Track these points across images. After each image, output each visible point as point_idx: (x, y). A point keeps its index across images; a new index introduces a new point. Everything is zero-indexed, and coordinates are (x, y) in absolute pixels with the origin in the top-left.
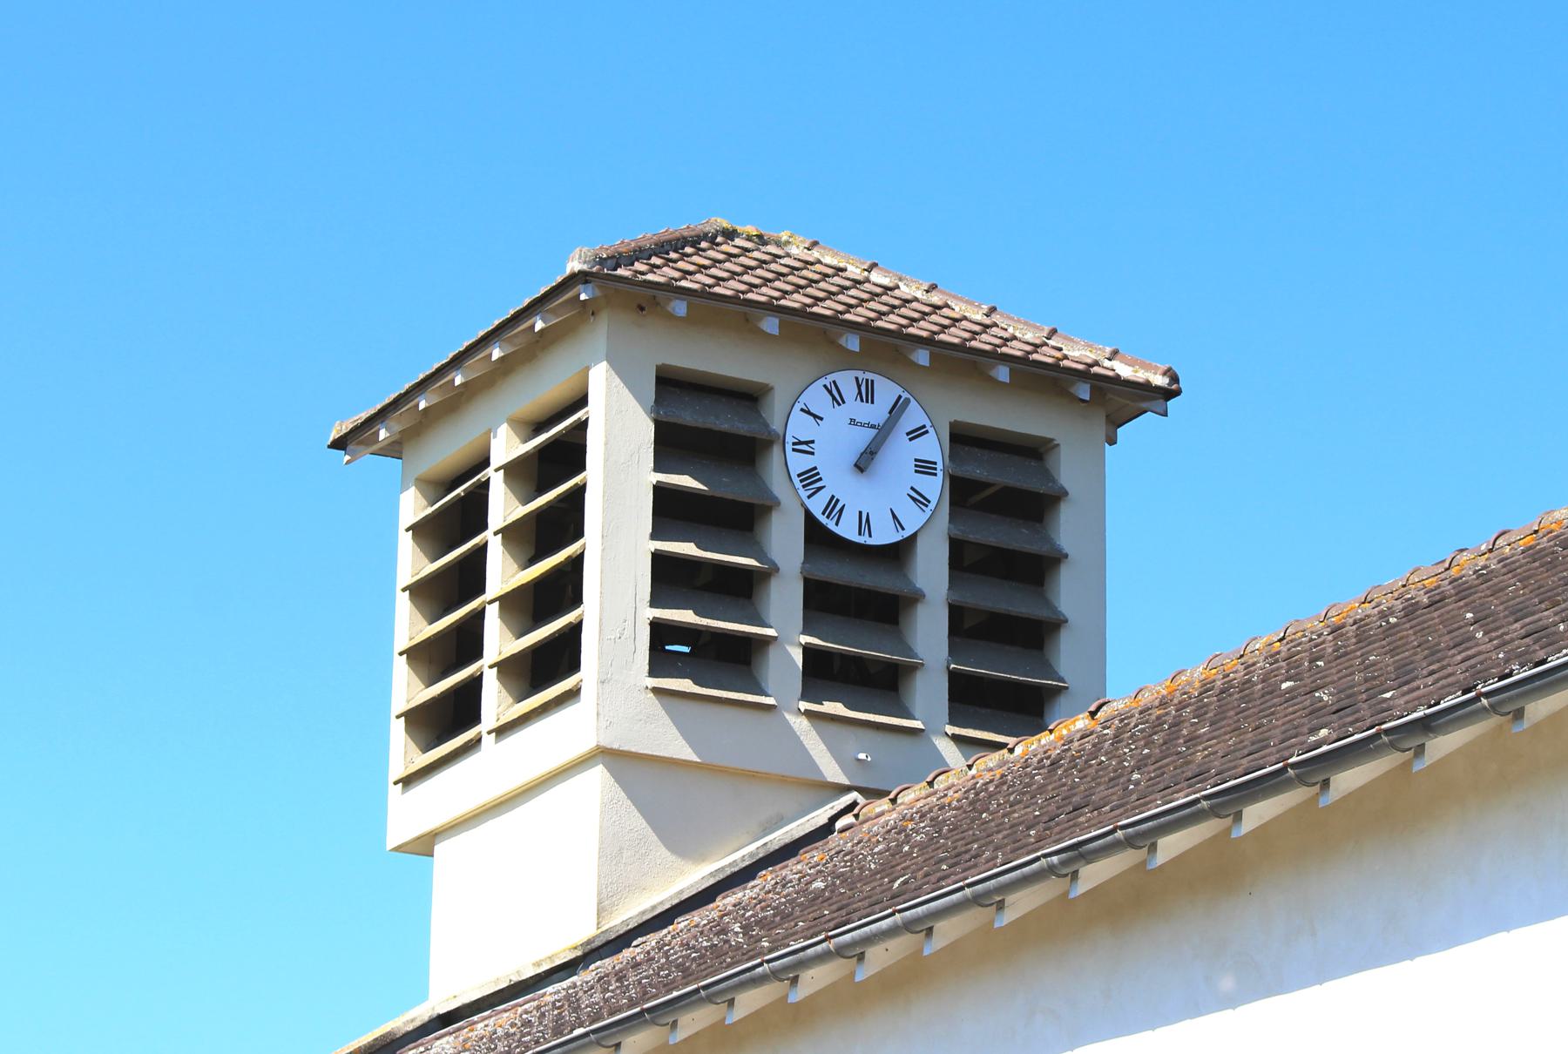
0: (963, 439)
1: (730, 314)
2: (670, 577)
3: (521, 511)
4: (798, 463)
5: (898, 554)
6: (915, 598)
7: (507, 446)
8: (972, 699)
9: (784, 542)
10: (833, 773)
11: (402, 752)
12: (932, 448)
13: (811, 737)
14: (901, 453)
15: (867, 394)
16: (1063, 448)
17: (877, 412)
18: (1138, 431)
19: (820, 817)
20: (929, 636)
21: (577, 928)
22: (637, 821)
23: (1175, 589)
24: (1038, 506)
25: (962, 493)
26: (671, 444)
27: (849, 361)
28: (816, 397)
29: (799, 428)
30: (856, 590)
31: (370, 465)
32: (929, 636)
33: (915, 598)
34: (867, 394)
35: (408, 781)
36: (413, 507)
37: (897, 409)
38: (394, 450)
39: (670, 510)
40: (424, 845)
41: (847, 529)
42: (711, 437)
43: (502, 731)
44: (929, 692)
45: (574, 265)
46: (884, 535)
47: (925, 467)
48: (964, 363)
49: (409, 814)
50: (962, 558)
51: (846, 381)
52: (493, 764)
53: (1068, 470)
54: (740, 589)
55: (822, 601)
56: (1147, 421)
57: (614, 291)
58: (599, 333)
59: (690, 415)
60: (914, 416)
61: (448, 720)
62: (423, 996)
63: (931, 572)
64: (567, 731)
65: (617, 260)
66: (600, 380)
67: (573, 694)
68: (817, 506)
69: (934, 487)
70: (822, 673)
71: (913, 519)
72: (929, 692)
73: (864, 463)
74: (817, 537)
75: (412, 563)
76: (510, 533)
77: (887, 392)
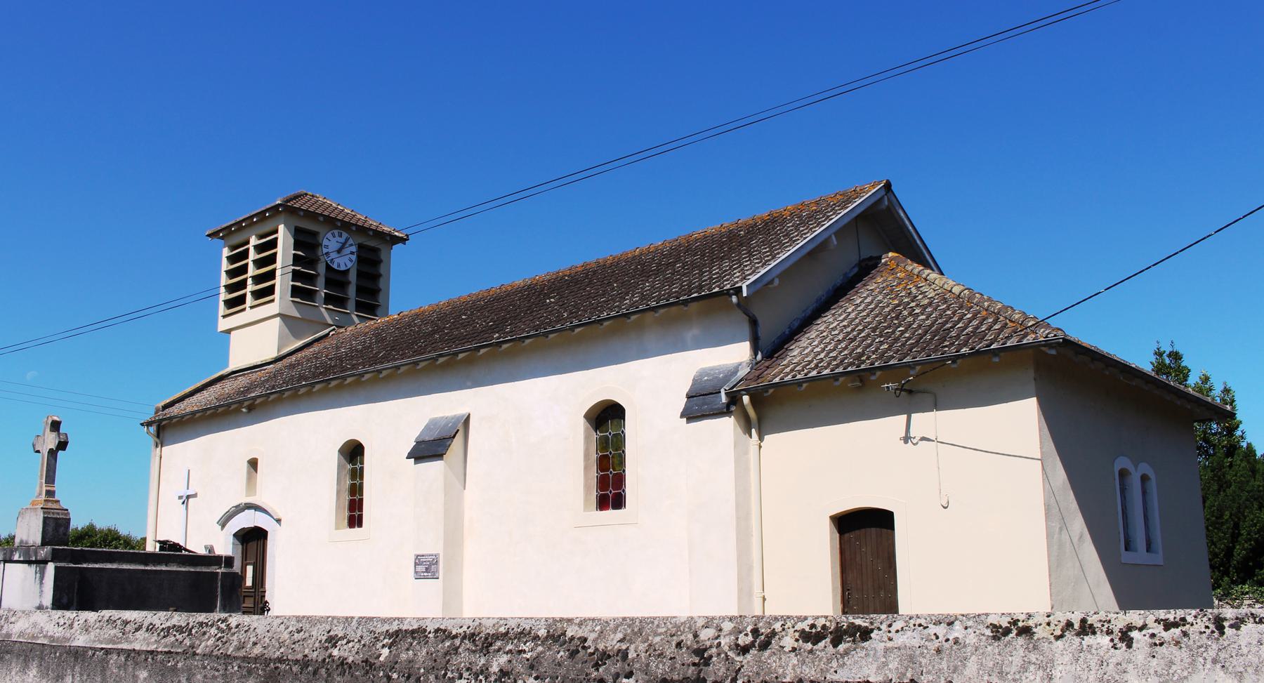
0: (360, 246)
1: (311, 216)
2: (296, 276)
3: (259, 256)
4: (325, 251)
5: (346, 272)
6: (349, 283)
7: (254, 241)
8: (360, 307)
9: (321, 269)
10: (330, 322)
11: (222, 309)
12: (354, 249)
13: (324, 312)
14: (347, 251)
15: (340, 236)
16: (586, 508)
17: (342, 240)
18: (397, 248)
19: (327, 331)
20: (352, 291)
21: (272, 354)
22: (287, 331)
23: (412, 289)
24: (376, 263)
25: (360, 260)
26: (297, 246)
27: (337, 228)
28: (329, 235)
29: (325, 242)
30: (336, 280)
31: (216, 240)
32: (352, 291)
33: (349, 283)
34: (340, 236)
35: (224, 317)
36: (226, 252)
37: (347, 240)
38: (222, 238)
39: (297, 260)
40: (229, 331)
41: (335, 266)
42: (306, 243)
43: (252, 307)
44: (351, 304)
45: (279, 202)
46: (343, 268)
47: (352, 253)
48: (362, 230)
49: (223, 324)
50: (360, 274)
51: (336, 232)
52: (248, 315)
53: (383, 256)
54: (310, 279)
55: (329, 283)
56: (400, 245)
57: (286, 210)
58: (282, 217)
59: (301, 238)
60: (351, 241)
61: (235, 303)
62: (227, 366)
63: (353, 277)
64: (273, 308)
65: (288, 201)
66: (281, 228)
67: (273, 301)
68: (328, 260)
69: (354, 257)
70: (328, 299)
71: (349, 265)
72: (351, 304)
73: (339, 251)
74: (328, 267)
75: (225, 265)
76: (254, 261)
77: (345, 235)
